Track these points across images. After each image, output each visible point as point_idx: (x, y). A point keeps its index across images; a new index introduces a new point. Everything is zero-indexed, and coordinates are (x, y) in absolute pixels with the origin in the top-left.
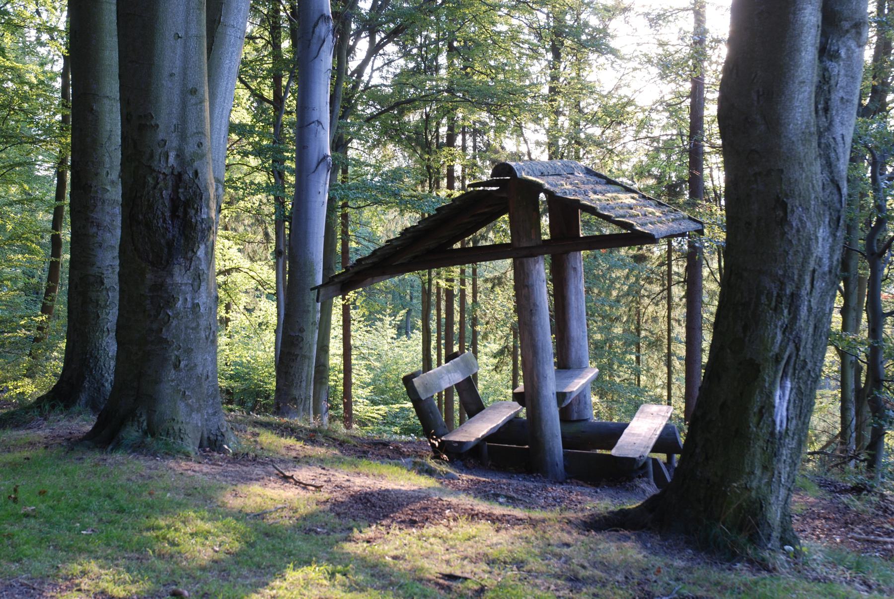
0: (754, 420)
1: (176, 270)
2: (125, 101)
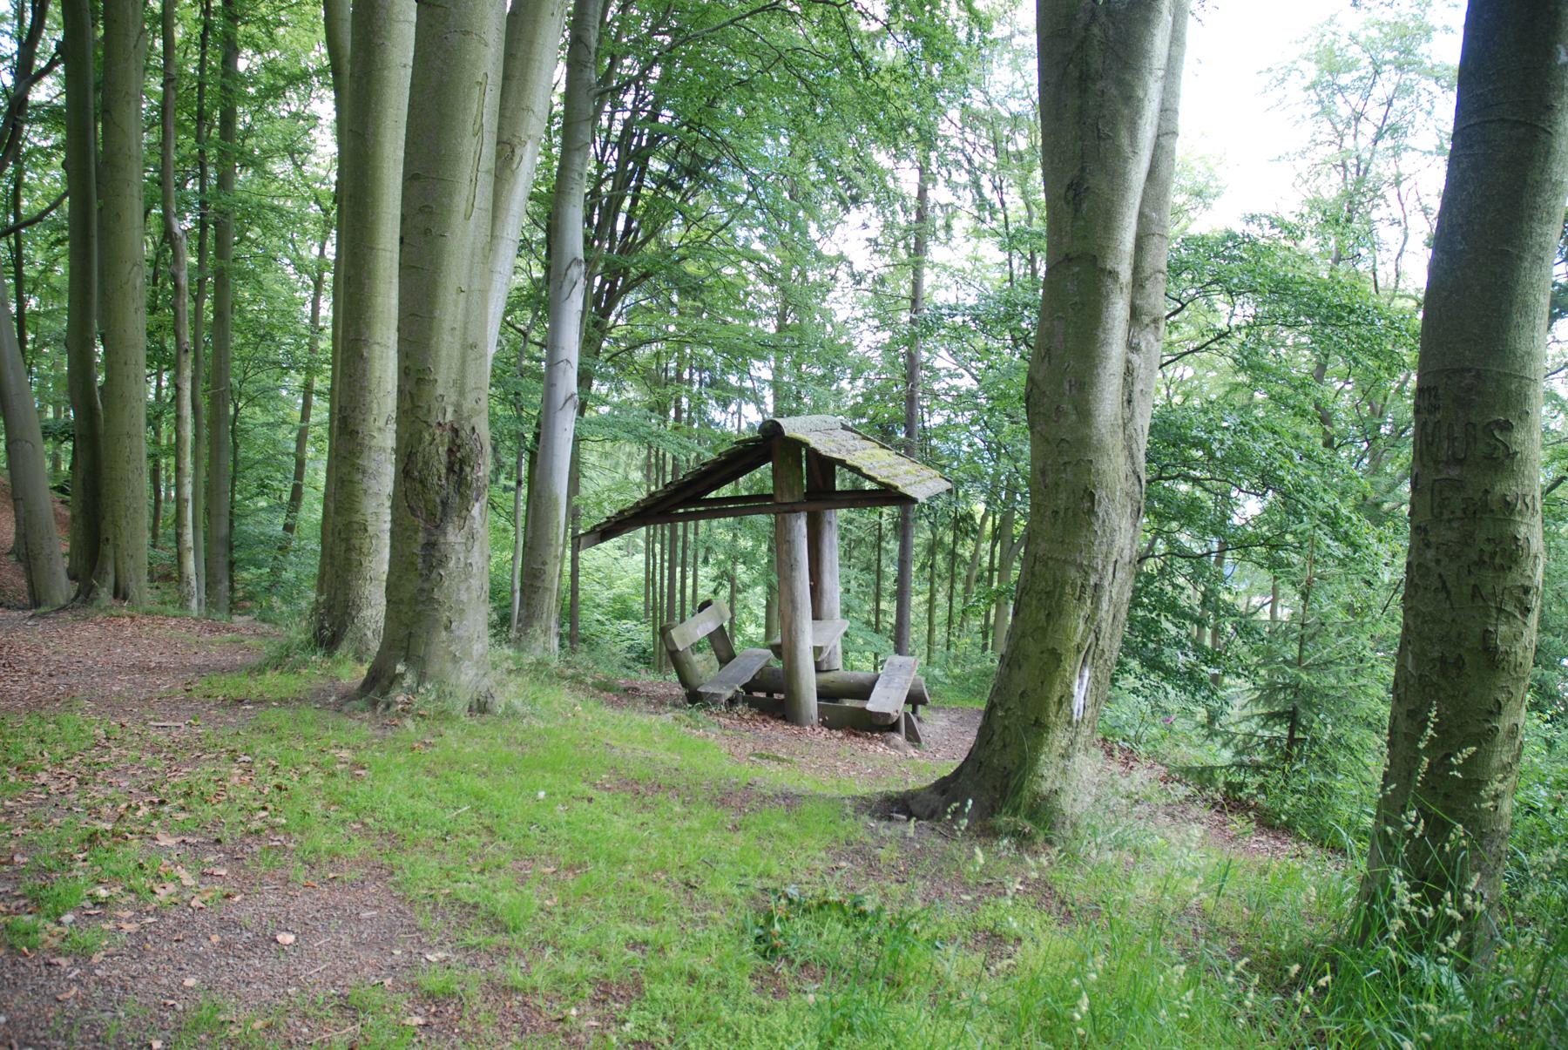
0: (1053, 708)
1: (450, 529)
2: (404, 355)
